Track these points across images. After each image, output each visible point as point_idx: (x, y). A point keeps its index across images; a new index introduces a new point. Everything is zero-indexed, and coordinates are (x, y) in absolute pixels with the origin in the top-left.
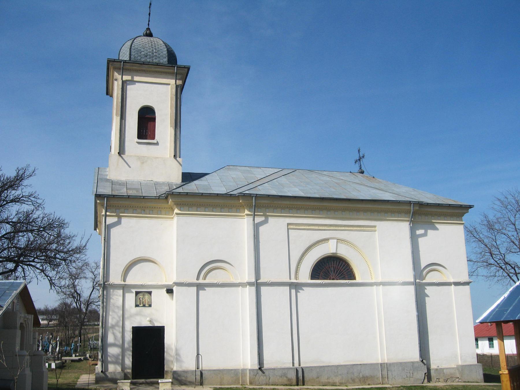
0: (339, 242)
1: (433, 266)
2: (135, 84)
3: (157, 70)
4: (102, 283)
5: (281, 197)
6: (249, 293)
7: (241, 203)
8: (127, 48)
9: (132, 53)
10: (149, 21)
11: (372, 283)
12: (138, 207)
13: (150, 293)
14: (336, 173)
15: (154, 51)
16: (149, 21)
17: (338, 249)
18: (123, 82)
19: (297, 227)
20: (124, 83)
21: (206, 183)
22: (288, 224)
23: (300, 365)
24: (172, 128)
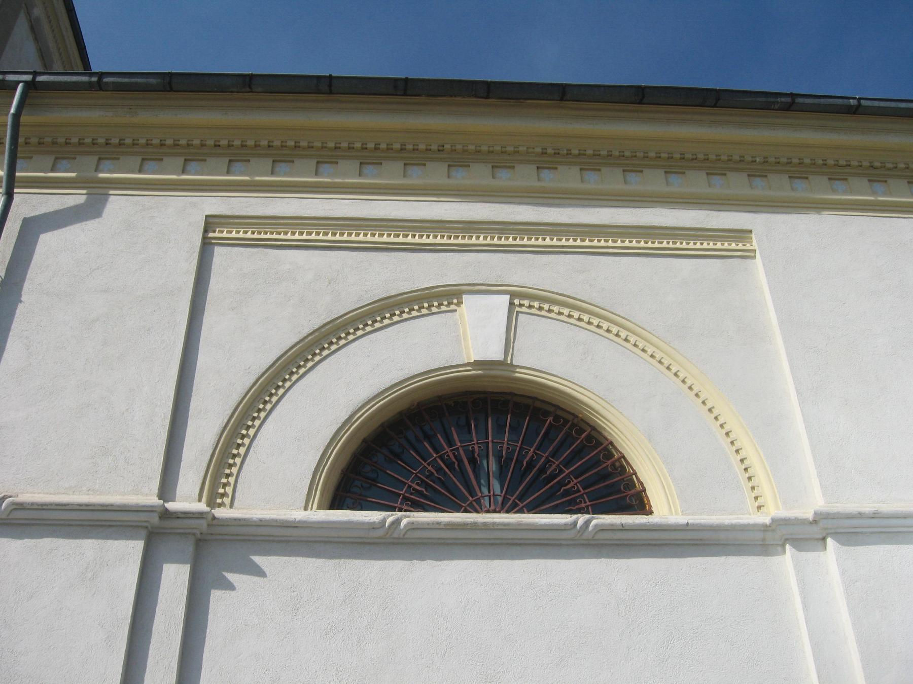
0: (524, 309)
17: (519, 345)
22: (210, 223)
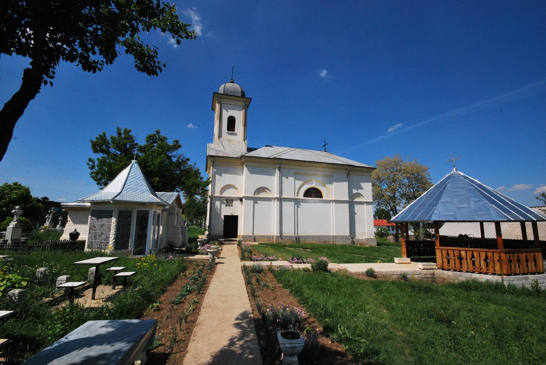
4: (211, 195)
21: (257, 152)
23: (297, 234)
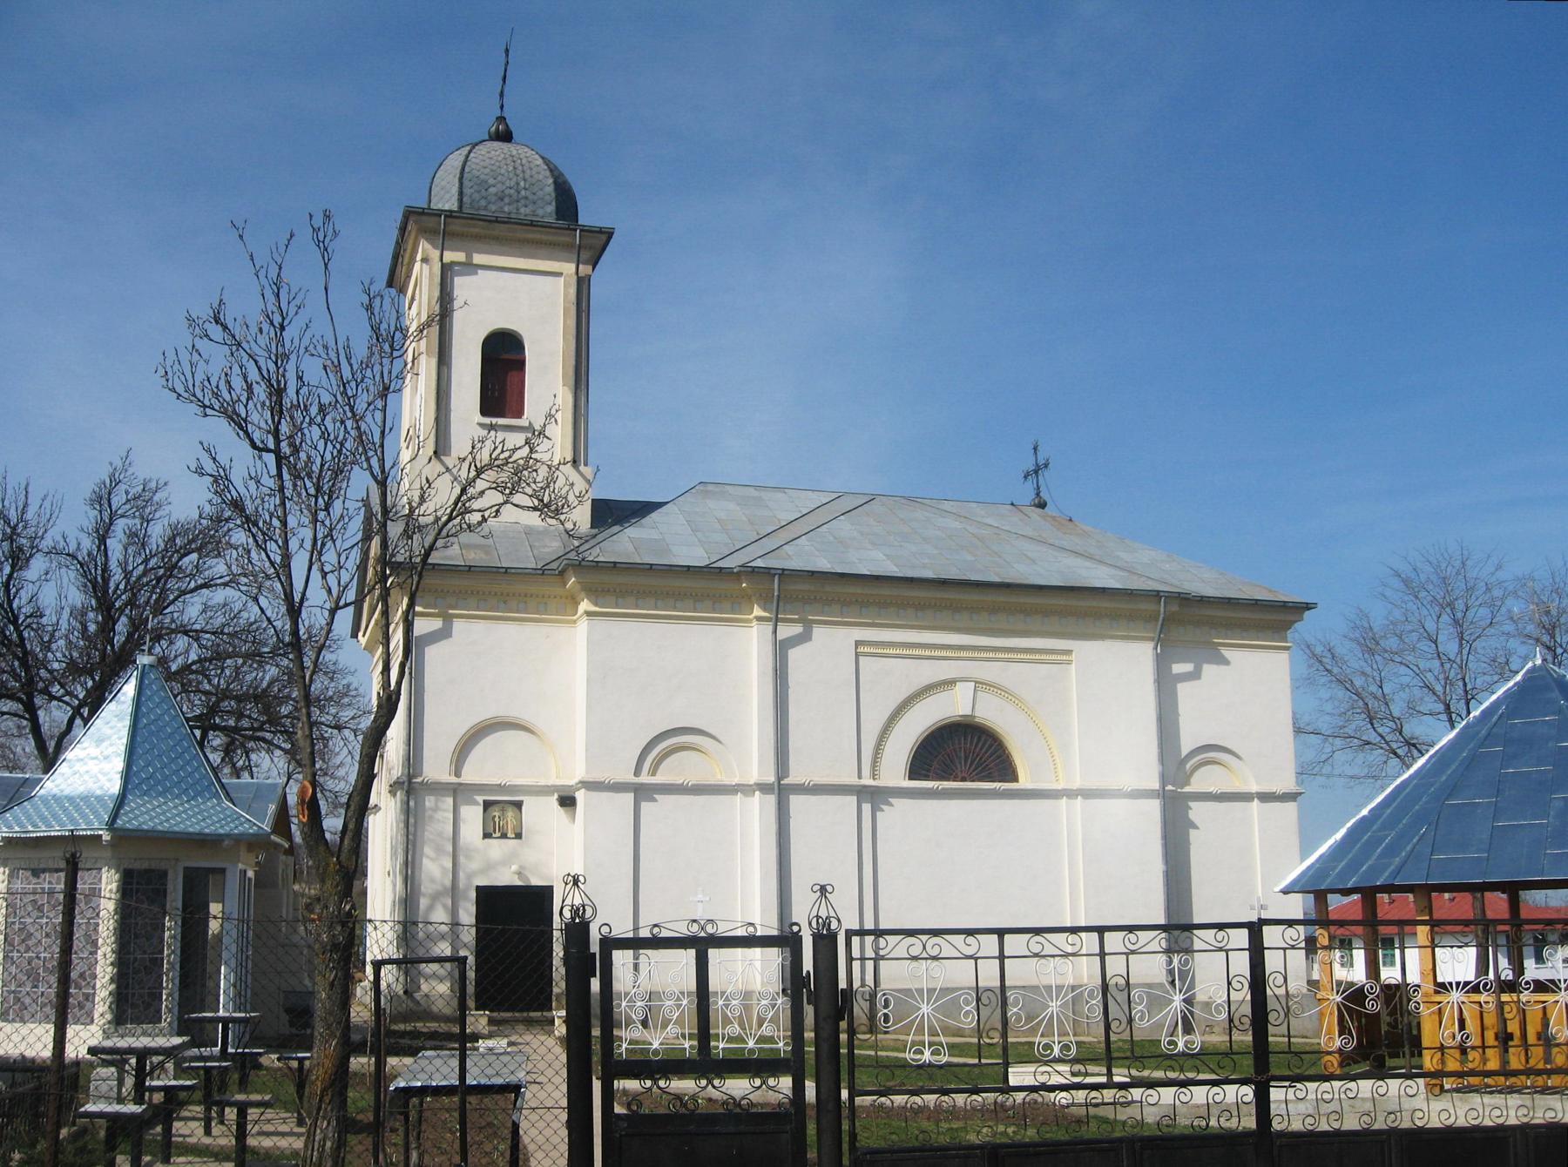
1: (1211, 752)
2: (477, 273)
3: (530, 236)
5: (843, 575)
6: (757, 813)
7: (744, 589)
8: (451, 176)
9: (467, 191)
10: (502, 95)
11: (1058, 790)
12: (490, 593)
13: (518, 805)
14: (974, 505)
15: (522, 184)
16: (502, 95)
18: (443, 266)
19: (879, 651)
20: (447, 271)
21: (654, 535)
22: (858, 643)
24: (566, 388)
